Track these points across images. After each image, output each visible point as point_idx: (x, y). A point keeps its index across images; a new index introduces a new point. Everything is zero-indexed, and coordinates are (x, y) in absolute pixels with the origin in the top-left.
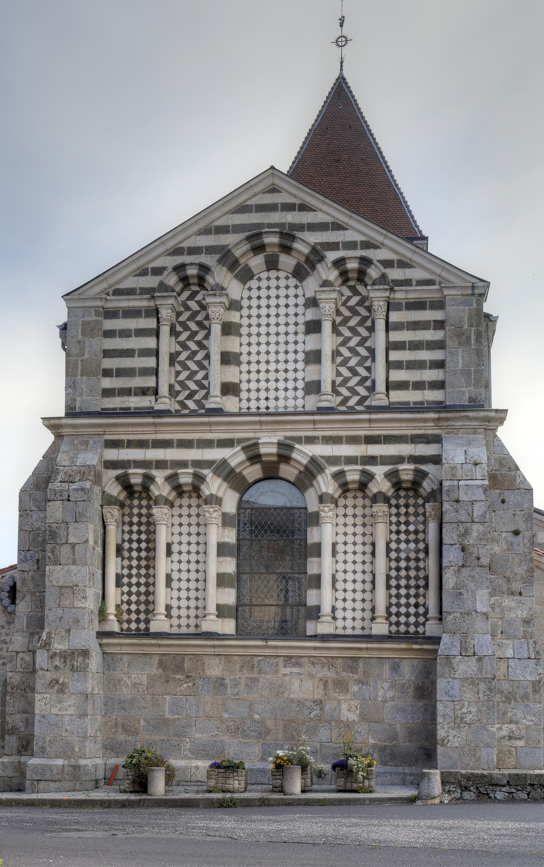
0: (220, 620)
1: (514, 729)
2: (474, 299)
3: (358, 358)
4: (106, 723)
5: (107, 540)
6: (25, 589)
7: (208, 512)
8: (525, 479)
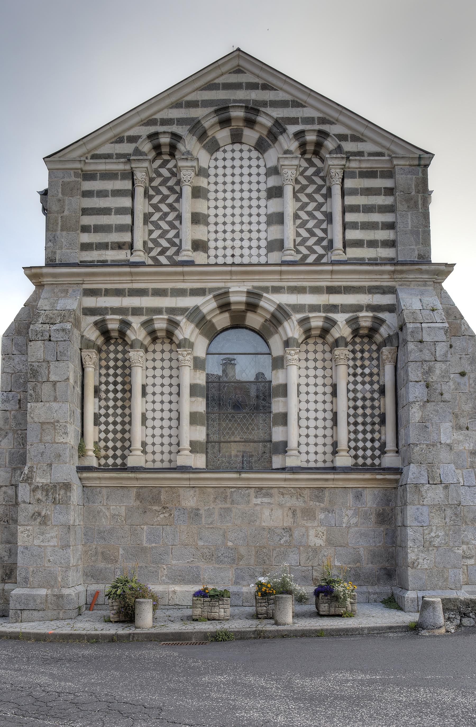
0: (193, 455)
1: (465, 549)
2: (420, 169)
3: (315, 221)
4: (86, 552)
5: (86, 381)
6: (7, 427)
7: (182, 355)
8: (469, 327)
